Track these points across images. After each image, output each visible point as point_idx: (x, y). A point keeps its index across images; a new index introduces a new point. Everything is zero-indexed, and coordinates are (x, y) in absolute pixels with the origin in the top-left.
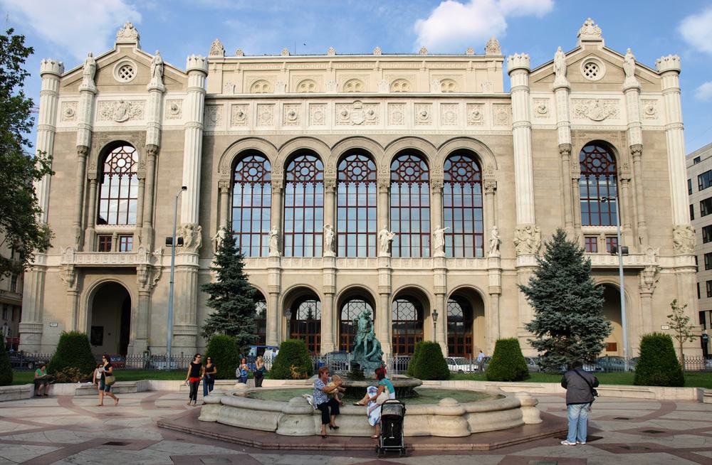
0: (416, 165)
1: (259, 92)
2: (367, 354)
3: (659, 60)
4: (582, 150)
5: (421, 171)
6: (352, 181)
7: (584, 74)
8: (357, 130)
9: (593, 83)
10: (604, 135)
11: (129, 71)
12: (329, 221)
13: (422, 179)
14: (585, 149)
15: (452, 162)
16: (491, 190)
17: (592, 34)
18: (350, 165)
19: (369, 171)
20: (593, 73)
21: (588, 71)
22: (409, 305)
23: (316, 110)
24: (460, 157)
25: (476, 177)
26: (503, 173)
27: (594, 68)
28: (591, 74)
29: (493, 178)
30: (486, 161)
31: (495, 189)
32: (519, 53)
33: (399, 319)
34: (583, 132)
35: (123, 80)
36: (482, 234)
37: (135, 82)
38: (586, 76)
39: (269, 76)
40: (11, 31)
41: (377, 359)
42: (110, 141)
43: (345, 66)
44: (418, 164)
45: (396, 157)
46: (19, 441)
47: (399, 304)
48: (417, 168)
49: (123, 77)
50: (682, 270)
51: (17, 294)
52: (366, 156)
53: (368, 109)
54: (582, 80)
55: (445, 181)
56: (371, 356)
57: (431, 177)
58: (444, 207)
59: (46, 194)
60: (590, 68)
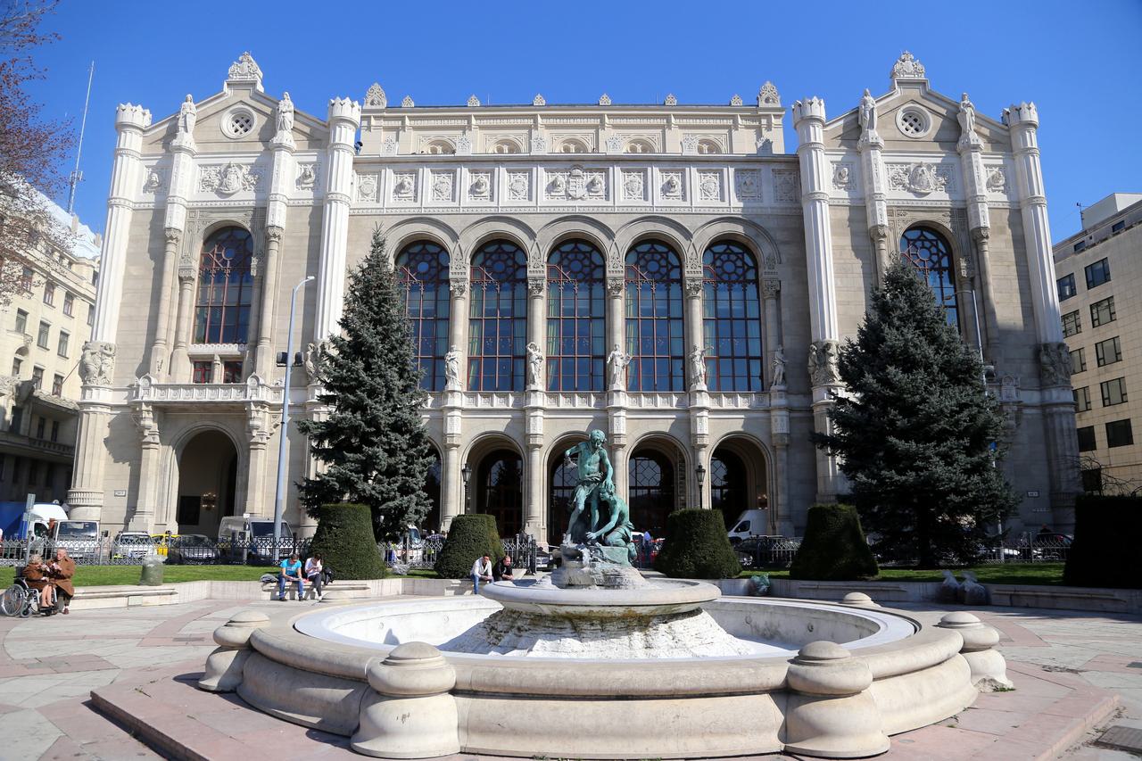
0: (509, 257)
3: (123, 107)
4: (903, 235)
8: (577, 206)
9: (916, 140)
11: (913, 123)
13: (518, 277)
14: (906, 234)
19: (593, 266)
23: (517, 178)
24: (725, 247)
25: (751, 275)
26: (451, 276)
29: (775, 276)
31: (778, 292)
33: (639, 485)
36: (760, 358)
42: (214, 221)
44: (665, 255)
47: (638, 462)
48: (663, 263)
50: (1062, 409)
51: (23, 437)
53: (587, 178)
54: (899, 136)
57: (608, 275)
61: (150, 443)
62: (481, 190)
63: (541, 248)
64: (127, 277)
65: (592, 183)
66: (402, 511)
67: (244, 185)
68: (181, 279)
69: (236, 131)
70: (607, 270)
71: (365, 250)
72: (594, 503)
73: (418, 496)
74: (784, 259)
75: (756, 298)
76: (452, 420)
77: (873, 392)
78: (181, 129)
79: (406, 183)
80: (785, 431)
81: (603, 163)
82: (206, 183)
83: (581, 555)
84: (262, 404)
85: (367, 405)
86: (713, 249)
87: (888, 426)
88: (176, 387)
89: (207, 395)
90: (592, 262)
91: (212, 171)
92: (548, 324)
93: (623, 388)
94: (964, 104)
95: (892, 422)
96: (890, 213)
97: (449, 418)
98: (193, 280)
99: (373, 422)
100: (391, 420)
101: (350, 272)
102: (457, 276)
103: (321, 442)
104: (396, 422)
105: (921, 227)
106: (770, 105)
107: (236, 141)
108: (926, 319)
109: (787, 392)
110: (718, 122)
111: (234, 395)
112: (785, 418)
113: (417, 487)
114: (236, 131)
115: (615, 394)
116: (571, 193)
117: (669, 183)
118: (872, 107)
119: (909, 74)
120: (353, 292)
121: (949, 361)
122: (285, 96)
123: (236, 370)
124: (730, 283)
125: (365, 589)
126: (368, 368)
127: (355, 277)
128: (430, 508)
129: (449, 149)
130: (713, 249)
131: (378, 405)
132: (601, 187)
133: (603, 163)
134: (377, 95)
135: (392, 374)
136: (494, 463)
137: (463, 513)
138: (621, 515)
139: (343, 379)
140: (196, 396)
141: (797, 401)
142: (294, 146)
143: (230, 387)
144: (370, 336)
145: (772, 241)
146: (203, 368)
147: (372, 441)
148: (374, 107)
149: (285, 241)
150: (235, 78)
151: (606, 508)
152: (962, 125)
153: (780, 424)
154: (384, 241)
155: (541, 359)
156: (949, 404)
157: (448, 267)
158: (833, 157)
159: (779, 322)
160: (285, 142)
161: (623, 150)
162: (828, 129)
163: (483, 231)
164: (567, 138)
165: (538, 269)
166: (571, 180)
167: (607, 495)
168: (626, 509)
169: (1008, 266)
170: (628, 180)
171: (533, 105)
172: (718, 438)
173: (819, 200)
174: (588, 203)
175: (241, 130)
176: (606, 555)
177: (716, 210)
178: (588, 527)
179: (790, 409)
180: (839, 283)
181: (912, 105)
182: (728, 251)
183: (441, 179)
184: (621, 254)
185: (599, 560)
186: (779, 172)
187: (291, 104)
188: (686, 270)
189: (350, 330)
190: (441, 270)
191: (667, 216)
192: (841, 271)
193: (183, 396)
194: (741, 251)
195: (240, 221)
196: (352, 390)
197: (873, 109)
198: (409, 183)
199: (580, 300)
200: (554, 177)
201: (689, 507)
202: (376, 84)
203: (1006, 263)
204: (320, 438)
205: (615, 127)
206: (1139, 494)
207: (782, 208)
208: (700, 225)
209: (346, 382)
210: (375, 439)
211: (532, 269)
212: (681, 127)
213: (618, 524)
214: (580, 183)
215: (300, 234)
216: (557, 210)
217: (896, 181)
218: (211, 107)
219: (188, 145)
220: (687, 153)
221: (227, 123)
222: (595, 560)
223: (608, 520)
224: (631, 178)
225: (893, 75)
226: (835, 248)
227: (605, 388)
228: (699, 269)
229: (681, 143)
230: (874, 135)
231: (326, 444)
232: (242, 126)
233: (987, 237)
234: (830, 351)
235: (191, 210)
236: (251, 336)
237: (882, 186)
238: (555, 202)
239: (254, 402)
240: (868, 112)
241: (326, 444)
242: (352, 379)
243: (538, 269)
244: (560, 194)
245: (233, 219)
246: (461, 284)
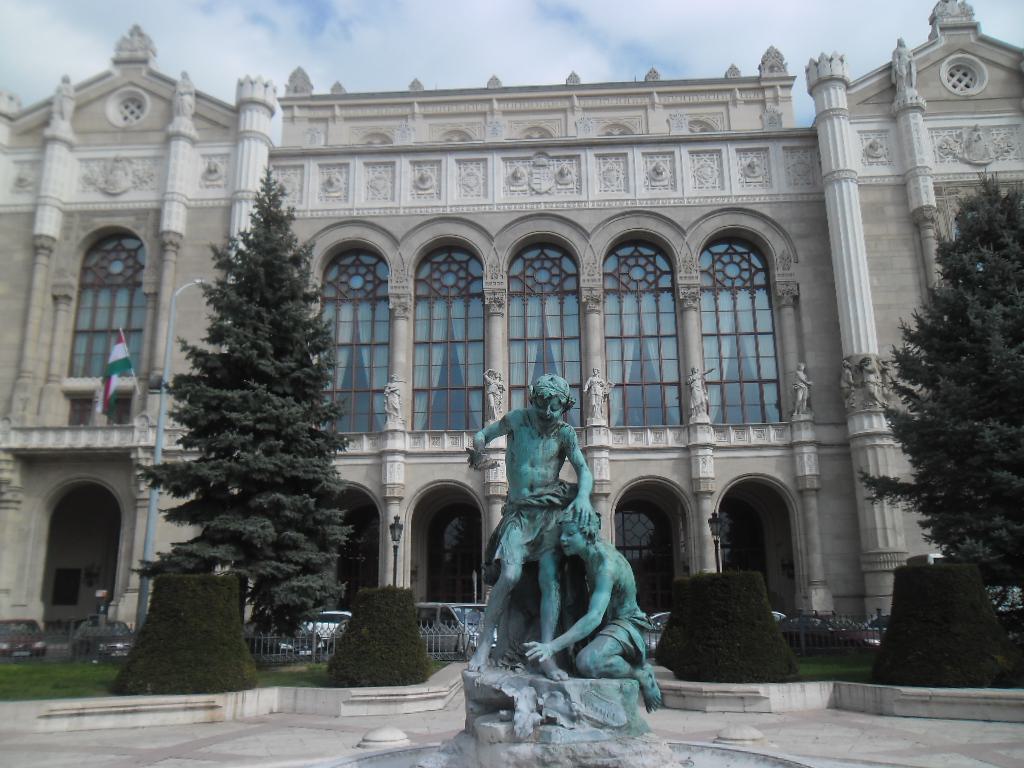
2: (561, 629)
5: (658, 273)
6: (724, 288)
8: (542, 204)
9: (967, 99)
11: (964, 83)
12: (597, 362)
15: (713, 254)
16: (788, 299)
17: (957, 16)
18: (730, 254)
23: (469, 171)
26: (390, 291)
27: (965, 75)
29: (789, 279)
30: (777, 246)
31: (796, 298)
33: (627, 545)
35: (945, 81)
38: (952, 89)
40: (66, 80)
41: (618, 661)
42: (96, 228)
44: (651, 259)
45: (707, 247)
46: (241, 737)
49: (952, 75)
53: (555, 167)
54: (945, 95)
55: (607, 292)
56: (583, 643)
57: (582, 285)
58: (387, 344)
60: (959, 75)
61: (8, 501)
62: (426, 187)
63: (499, 254)
65: (561, 174)
67: (134, 183)
68: (55, 298)
70: (582, 278)
72: (548, 568)
74: (801, 256)
75: (767, 307)
76: (392, 466)
78: (56, 116)
79: (334, 180)
80: (814, 472)
81: (573, 148)
82: (88, 181)
83: (509, 705)
88: (44, 429)
89: (83, 440)
90: (562, 270)
92: (509, 345)
96: (938, 191)
97: (388, 465)
109: (815, 423)
110: (712, 98)
111: (116, 440)
112: (813, 455)
115: (594, 430)
116: (536, 187)
117: (655, 170)
118: (909, 59)
124: (734, 291)
125: (213, 708)
129: (386, 139)
133: (573, 148)
136: (448, 522)
138: (618, 592)
140: (68, 440)
141: (828, 435)
142: (193, 133)
143: (113, 428)
145: (785, 235)
146: (80, 405)
149: (187, 251)
151: (578, 574)
153: (809, 464)
158: (861, 125)
159: (800, 336)
160: (183, 130)
161: (594, 134)
162: (853, 91)
163: (426, 237)
165: (496, 281)
166: (534, 171)
167: (579, 539)
172: (731, 478)
175: (131, 117)
176: (579, 706)
178: (532, 627)
179: (818, 444)
180: (875, 282)
181: (960, 55)
182: (730, 251)
183: (377, 174)
184: (598, 258)
185: (562, 720)
186: (792, 149)
188: (679, 275)
190: (379, 285)
191: (653, 210)
192: (877, 267)
193: (50, 441)
194: (653, 253)
197: (910, 62)
198: (338, 180)
200: (513, 169)
201: (694, 571)
205: (585, 109)
207: (797, 195)
208: (694, 219)
211: (489, 280)
212: (666, 106)
213: (611, 616)
217: (944, 151)
219: (914, 101)
220: (675, 132)
222: (551, 721)
226: (868, 238)
229: (668, 121)
230: (911, 94)
232: (132, 113)
234: (870, 368)
235: (68, 215)
237: (927, 158)
238: (516, 199)
239: (142, 447)
240: (904, 67)
246: (403, 300)
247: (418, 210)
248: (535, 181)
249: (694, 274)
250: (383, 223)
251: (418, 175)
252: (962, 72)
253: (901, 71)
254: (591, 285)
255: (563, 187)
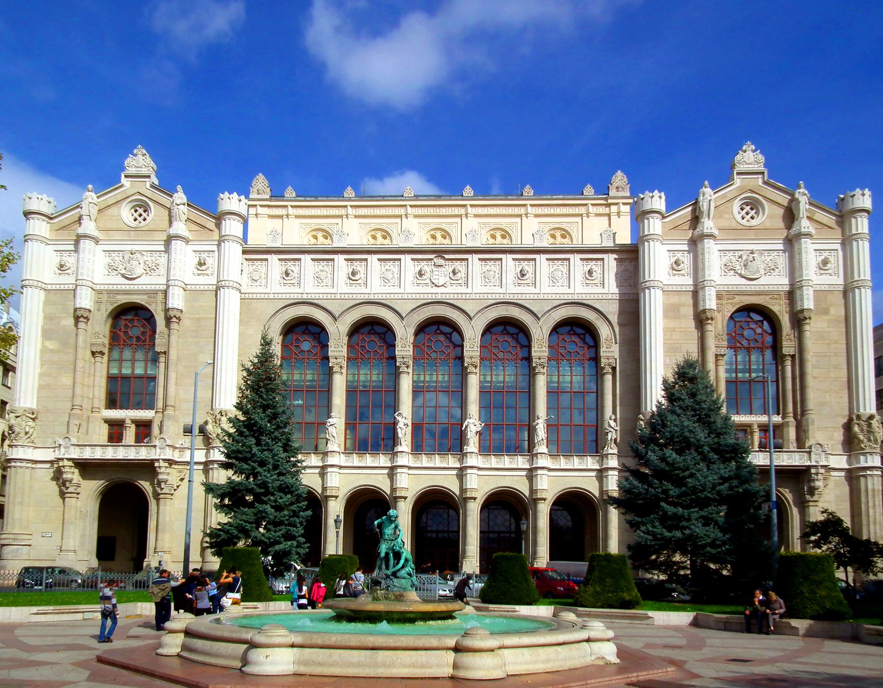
1: (381, 243)
2: (394, 567)
4: (731, 317)
7: (739, 217)
8: (439, 293)
9: (750, 228)
10: (762, 297)
11: (750, 215)
17: (751, 164)
20: (138, 217)
21: (136, 215)
22: (503, 512)
23: (387, 267)
26: (330, 354)
28: (140, 219)
29: (610, 354)
32: (862, 189)
34: (731, 294)
37: (152, 227)
39: (507, 223)
42: (120, 303)
43: (571, 210)
47: (490, 511)
49: (742, 209)
52: (583, 329)
54: (734, 225)
59: (784, 390)
64: (44, 350)
66: (287, 554)
69: (135, 220)
71: (256, 349)
73: (298, 542)
77: (654, 466)
82: (112, 268)
84: (171, 462)
85: (258, 472)
86: (557, 330)
87: (661, 494)
91: (118, 258)
93: (476, 450)
94: (799, 193)
95: (666, 492)
96: (719, 296)
98: (104, 354)
99: (264, 485)
100: (277, 483)
101: (243, 366)
102: (335, 354)
103: (222, 500)
104: (281, 485)
105: (747, 309)
106: (620, 194)
107: (136, 230)
108: (704, 409)
111: (143, 454)
113: (297, 534)
114: (135, 220)
116: (434, 281)
118: (710, 198)
119: (749, 164)
120: (245, 382)
121: (718, 443)
122: (178, 189)
123: (144, 430)
126: (258, 443)
127: (247, 370)
128: (307, 550)
130: (557, 330)
131: (266, 473)
132: (461, 275)
134: (260, 183)
135: (278, 448)
137: (341, 552)
138: (406, 560)
139: (239, 451)
144: (260, 418)
146: (116, 432)
147: (263, 500)
148: (259, 197)
150: (131, 171)
151: (398, 555)
152: (795, 212)
154: (271, 341)
155: (408, 426)
156: (713, 478)
157: (328, 346)
161: (482, 240)
164: (434, 227)
165: (405, 349)
168: (410, 557)
169: (828, 344)
170: (485, 269)
171: (403, 196)
172: (555, 492)
173: (648, 288)
174: (451, 291)
177: (562, 296)
181: (749, 195)
187: (184, 196)
189: (245, 413)
195: (143, 303)
196: (245, 460)
199: (440, 376)
200: (420, 267)
202: (260, 174)
203: (827, 342)
204: (222, 497)
206: (881, 542)
209: (241, 454)
210: (265, 499)
211: (468, 349)
214: (441, 275)
215: (197, 316)
216: (422, 296)
217: (728, 268)
218: (112, 197)
221: (126, 213)
223: (398, 563)
224: (488, 267)
225: (733, 167)
226: (666, 330)
227: (461, 450)
228: (544, 349)
231: (226, 501)
233: (810, 318)
236: (160, 404)
241: (226, 501)
242: (246, 452)
243: (405, 349)
244: (425, 282)
245: (138, 301)
247: (596, 296)
248: (435, 277)
249: (544, 349)
250: (597, 306)
251: (351, 270)
252: (749, 207)
253: (702, 205)
254: (472, 354)
255: (454, 282)
